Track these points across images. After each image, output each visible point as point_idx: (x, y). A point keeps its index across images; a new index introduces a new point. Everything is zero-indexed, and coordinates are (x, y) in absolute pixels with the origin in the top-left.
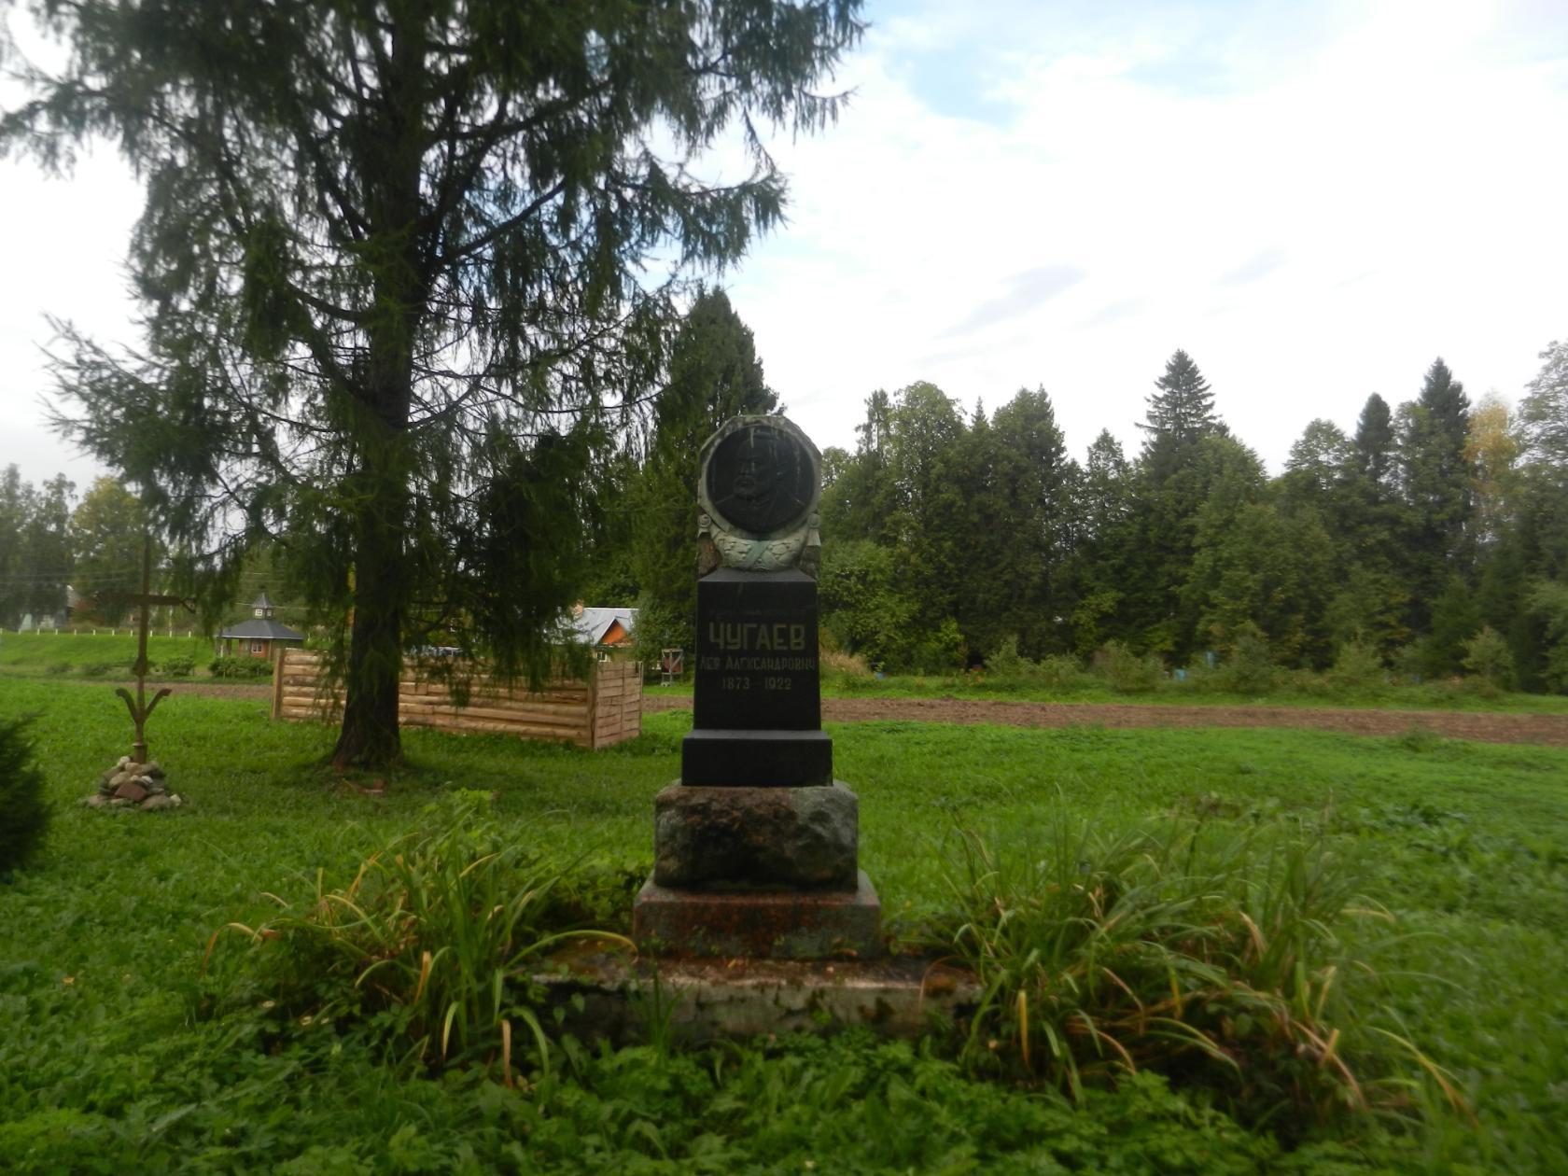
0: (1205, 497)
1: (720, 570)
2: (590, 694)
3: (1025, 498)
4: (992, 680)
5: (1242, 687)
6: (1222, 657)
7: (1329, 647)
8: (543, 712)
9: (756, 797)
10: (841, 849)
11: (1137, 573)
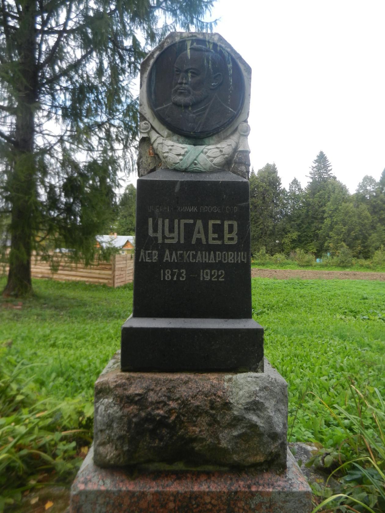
0: (329, 201)
1: (159, 170)
2: (113, 266)
3: (268, 200)
4: (256, 262)
5: (341, 265)
6: (333, 255)
7: (369, 251)
8: (94, 273)
9: (194, 385)
10: (274, 436)
11: (305, 226)
